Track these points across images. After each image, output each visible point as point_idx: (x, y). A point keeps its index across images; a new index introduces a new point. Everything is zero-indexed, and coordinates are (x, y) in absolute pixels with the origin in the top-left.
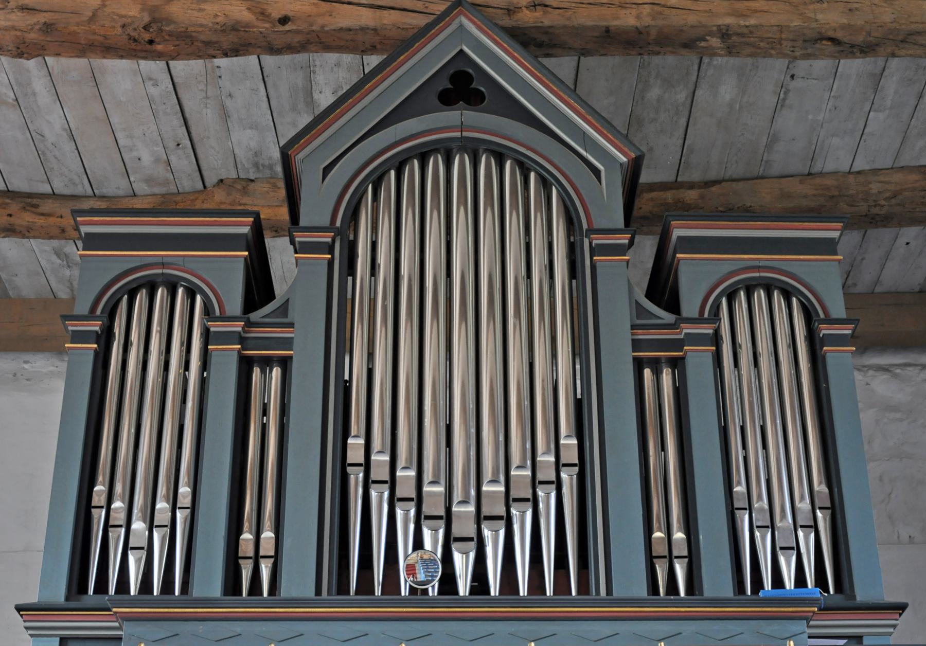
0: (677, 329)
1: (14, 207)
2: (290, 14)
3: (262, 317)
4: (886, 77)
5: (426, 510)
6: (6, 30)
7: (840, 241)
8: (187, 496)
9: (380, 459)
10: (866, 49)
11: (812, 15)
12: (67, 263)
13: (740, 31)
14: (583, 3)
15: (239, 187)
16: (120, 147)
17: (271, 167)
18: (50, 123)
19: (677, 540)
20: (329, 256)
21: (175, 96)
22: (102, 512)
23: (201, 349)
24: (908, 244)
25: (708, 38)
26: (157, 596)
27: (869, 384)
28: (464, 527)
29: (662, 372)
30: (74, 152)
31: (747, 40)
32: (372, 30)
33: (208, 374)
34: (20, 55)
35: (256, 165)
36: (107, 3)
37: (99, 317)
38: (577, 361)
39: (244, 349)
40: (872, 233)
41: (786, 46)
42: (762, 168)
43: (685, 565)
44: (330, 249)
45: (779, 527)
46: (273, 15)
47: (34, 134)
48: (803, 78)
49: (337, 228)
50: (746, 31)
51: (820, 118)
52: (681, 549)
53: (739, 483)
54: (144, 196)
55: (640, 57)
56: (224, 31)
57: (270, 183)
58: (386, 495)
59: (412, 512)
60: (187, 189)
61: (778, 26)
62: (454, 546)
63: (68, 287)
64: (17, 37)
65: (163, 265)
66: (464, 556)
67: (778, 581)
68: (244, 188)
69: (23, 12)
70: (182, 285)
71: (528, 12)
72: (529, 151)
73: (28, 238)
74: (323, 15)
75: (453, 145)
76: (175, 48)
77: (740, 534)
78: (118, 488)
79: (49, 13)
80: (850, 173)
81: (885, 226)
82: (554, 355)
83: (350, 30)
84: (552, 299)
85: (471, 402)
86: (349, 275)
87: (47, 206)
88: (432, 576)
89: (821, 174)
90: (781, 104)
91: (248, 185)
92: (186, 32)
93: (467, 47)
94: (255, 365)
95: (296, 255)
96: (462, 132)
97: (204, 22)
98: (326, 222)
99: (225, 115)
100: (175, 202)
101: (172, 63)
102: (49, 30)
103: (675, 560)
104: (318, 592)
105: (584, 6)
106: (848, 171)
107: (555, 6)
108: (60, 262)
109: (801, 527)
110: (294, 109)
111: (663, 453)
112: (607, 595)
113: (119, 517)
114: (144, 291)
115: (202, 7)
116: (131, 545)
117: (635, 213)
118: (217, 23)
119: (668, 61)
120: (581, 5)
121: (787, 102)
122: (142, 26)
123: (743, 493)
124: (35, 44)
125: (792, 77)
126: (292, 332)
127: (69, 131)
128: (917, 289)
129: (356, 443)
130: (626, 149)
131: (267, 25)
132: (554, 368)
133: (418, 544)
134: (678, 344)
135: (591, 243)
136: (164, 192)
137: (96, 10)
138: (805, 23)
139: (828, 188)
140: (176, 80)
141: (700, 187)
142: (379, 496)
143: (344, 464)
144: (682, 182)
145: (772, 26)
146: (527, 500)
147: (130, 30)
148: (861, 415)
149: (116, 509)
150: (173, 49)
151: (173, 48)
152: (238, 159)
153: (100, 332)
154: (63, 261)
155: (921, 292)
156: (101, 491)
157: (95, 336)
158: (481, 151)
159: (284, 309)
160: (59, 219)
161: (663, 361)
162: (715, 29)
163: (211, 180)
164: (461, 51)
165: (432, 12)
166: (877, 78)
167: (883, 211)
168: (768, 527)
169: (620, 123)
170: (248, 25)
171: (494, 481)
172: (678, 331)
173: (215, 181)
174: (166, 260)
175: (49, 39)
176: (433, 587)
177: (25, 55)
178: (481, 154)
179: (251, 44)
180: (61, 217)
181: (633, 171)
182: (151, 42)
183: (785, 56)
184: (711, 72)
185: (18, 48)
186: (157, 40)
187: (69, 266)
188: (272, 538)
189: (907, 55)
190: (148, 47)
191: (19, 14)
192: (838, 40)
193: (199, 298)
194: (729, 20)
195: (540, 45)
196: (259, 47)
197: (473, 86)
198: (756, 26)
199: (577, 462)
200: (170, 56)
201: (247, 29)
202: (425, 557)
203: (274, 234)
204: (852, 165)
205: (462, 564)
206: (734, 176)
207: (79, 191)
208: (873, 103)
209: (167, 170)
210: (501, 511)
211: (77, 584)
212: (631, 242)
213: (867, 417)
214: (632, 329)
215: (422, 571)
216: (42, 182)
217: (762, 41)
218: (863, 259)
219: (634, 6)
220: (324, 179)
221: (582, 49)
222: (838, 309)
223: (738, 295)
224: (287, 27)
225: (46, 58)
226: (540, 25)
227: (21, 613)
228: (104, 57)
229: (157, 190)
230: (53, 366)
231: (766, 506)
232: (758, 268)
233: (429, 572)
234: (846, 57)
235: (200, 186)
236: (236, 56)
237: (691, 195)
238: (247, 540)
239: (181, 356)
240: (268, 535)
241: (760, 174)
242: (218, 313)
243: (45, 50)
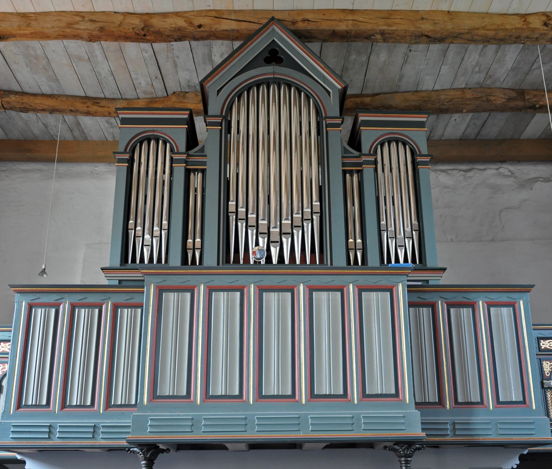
0: (360, 158)
1: (89, 104)
2: (202, 23)
3: (194, 153)
4: (448, 51)
5: (260, 230)
6: (84, 30)
7: (427, 123)
8: (166, 225)
9: (242, 210)
10: (441, 40)
11: (419, 26)
12: (112, 126)
13: (389, 32)
14: (324, 20)
15: (182, 95)
16: (132, 78)
17: (195, 87)
18: (103, 68)
19: (358, 242)
20: (220, 128)
21: (154, 57)
22: (132, 231)
23: (170, 166)
24: (455, 120)
25: (375, 35)
26: (156, 264)
27: (438, 177)
28: (275, 237)
29: (354, 176)
30: (113, 81)
31: (390, 36)
32: (237, 30)
33: (173, 178)
34: (90, 41)
35: (189, 86)
36: (126, 18)
37: (128, 152)
38: (320, 167)
39: (187, 165)
40: (441, 116)
41: (408, 39)
42: (397, 89)
43: (361, 252)
44: (221, 125)
45: (398, 238)
46: (195, 24)
47: (96, 73)
48: (415, 51)
49: (223, 116)
50: (391, 32)
51: (421, 68)
52: (359, 246)
53: (383, 220)
54: (143, 99)
55: (347, 43)
56: (175, 31)
57: (195, 94)
58: (244, 224)
59: (255, 231)
60: (160, 96)
61: (405, 30)
62: (271, 245)
63: (112, 136)
64: (89, 33)
65: (153, 131)
66: (275, 248)
67: (397, 260)
68: (184, 95)
69: (91, 22)
70: (161, 139)
71: (301, 23)
72: (301, 84)
73: (96, 116)
74: (216, 24)
75: (270, 81)
76: (155, 38)
77: (382, 238)
78: (139, 221)
79: (102, 23)
80: (433, 91)
81: (446, 113)
82: (311, 164)
83: (227, 31)
84: (310, 142)
85: (278, 187)
86: (229, 133)
87: (103, 103)
88: (262, 256)
89: (421, 91)
90: (405, 62)
91: (185, 94)
92: (159, 31)
93: (276, 38)
94: (192, 172)
95: (207, 127)
96: (274, 75)
97: (167, 27)
98: (219, 114)
99: (175, 65)
100: (155, 101)
101: (153, 44)
102: (102, 30)
103: (357, 251)
104: (218, 264)
105: (324, 21)
106: (432, 89)
107: (312, 21)
108: (109, 126)
109: (407, 238)
110: (204, 63)
111: (353, 207)
112: (331, 265)
113: (139, 233)
114: (146, 142)
115: (165, 20)
116: (145, 244)
117: (345, 107)
118: (172, 27)
119: (359, 44)
120: (323, 20)
121: (408, 61)
122: (141, 28)
123: (384, 224)
124: (96, 36)
125: (410, 50)
126: (205, 159)
127: (111, 72)
128: (459, 138)
129: (232, 203)
130: (341, 83)
131: (193, 28)
132: (311, 170)
133: (257, 244)
134: (360, 164)
135: (326, 123)
136: (151, 97)
137: (121, 21)
138: (415, 29)
139: (424, 97)
140: (155, 50)
141: (371, 96)
142: (242, 225)
143: (228, 212)
144: (364, 94)
145: (402, 30)
146: (300, 226)
147: (136, 30)
148: (432, 191)
149: (138, 230)
150: (154, 38)
151: (154, 38)
152: (181, 84)
153: (129, 159)
154: (110, 125)
155: (460, 139)
156: (132, 223)
157: (127, 160)
158: (281, 83)
159: (202, 150)
160: (108, 109)
161: (354, 171)
162: (379, 31)
163: (170, 92)
164: (274, 40)
165: (261, 23)
166: (445, 53)
167: (446, 107)
168: (394, 238)
169: (338, 72)
170: (185, 28)
171: (287, 219)
172: (360, 159)
173: (172, 92)
174: (154, 129)
175: (102, 34)
176: (263, 261)
177: (92, 41)
178: (281, 84)
179: (186, 36)
180: (109, 108)
181: (345, 89)
182: (145, 35)
183: (407, 43)
184: (376, 48)
185: (90, 38)
186: (147, 34)
187: (112, 127)
188: (200, 241)
189: (457, 43)
190: (143, 37)
191: (89, 23)
192: (429, 36)
193: (168, 144)
194: (384, 28)
195: (306, 37)
196: (189, 38)
197: (278, 55)
198: (396, 30)
199: (319, 211)
200: (153, 41)
201: (184, 30)
202: (260, 248)
203: (196, 115)
204: (434, 87)
205: (274, 252)
206: (385, 92)
207: (116, 96)
208: (443, 62)
209: (152, 88)
210: (290, 231)
211: (124, 259)
212: (342, 122)
213: (435, 192)
214: (342, 158)
215: (259, 254)
216: (101, 93)
217: (398, 36)
218: (437, 126)
219: (345, 21)
220: (218, 95)
221: (324, 39)
222: (424, 151)
223: (385, 144)
224: (202, 29)
225: (101, 42)
226: (306, 29)
227: (103, 271)
228: (125, 42)
229: (148, 96)
230: (107, 168)
231: (393, 229)
232: (393, 133)
233: (261, 254)
234: (432, 43)
235: (166, 95)
236: (180, 41)
237: (367, 100)
238: (190, 242)
239: (162, 168)
240: (198, 240)
241: (396, 91)
242: (176, 151)
243: (101, 38)
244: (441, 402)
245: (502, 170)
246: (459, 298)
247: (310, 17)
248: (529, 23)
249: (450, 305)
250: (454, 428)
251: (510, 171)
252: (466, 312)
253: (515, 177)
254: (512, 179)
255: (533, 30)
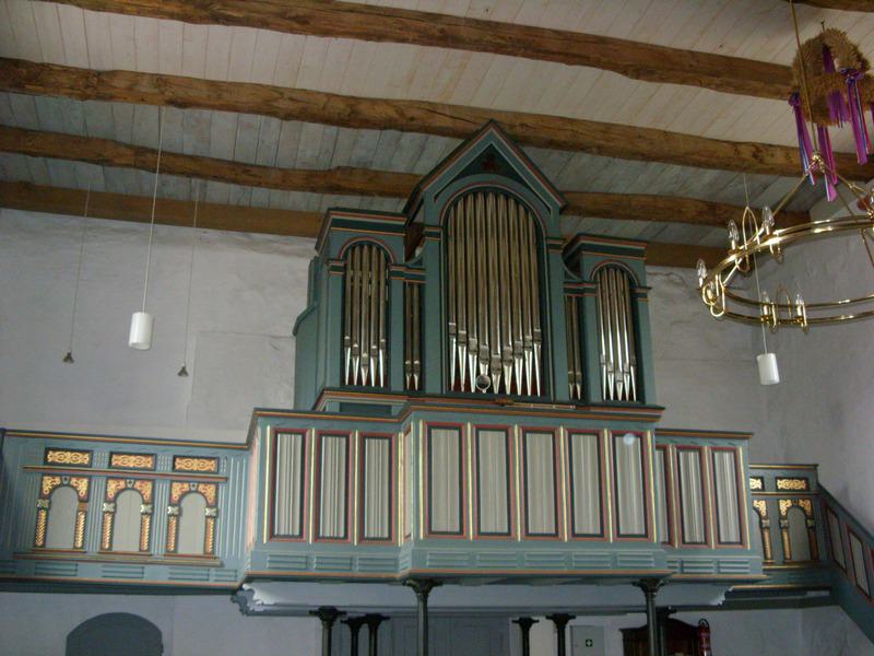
159: (420, 262)
170: (396, 120)
224: (414, 122)
244: (706, 542)
245: (673, 277)
246: (687, 442)
247: (528, 121)
248: (739, 153)
249: (680, 448)
250: (719, 567)
251: (681, 278)
252: (692, 456)
253: (687, 286)
254: (683, 288)
255: (744, 160)
